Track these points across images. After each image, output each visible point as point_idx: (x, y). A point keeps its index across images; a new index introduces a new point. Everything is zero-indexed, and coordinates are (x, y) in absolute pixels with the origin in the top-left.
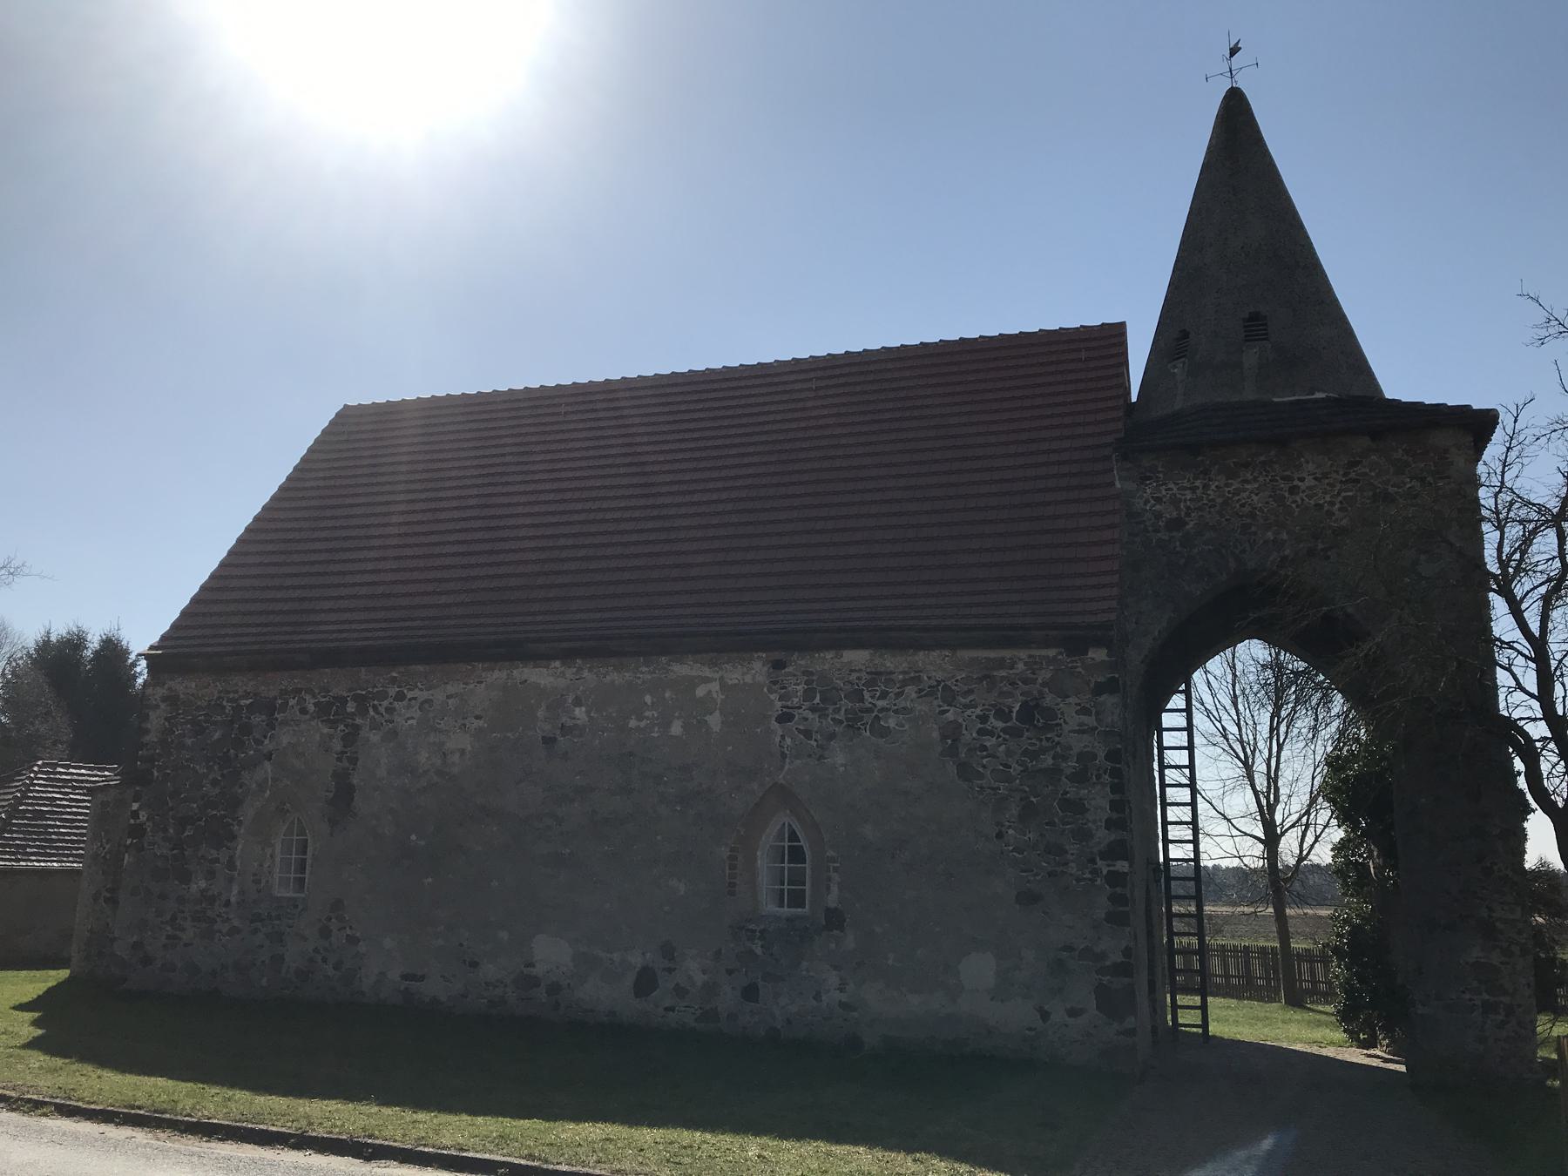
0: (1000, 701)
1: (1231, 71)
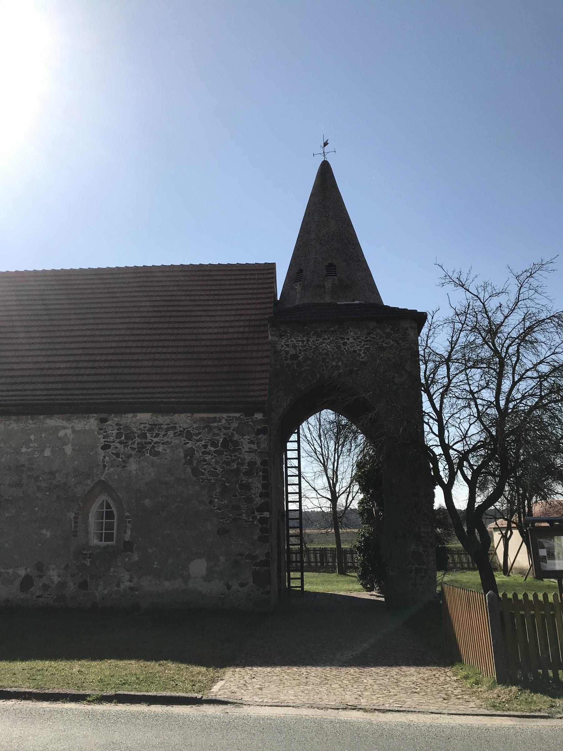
0: (214, 438)
1: (324, 153)
